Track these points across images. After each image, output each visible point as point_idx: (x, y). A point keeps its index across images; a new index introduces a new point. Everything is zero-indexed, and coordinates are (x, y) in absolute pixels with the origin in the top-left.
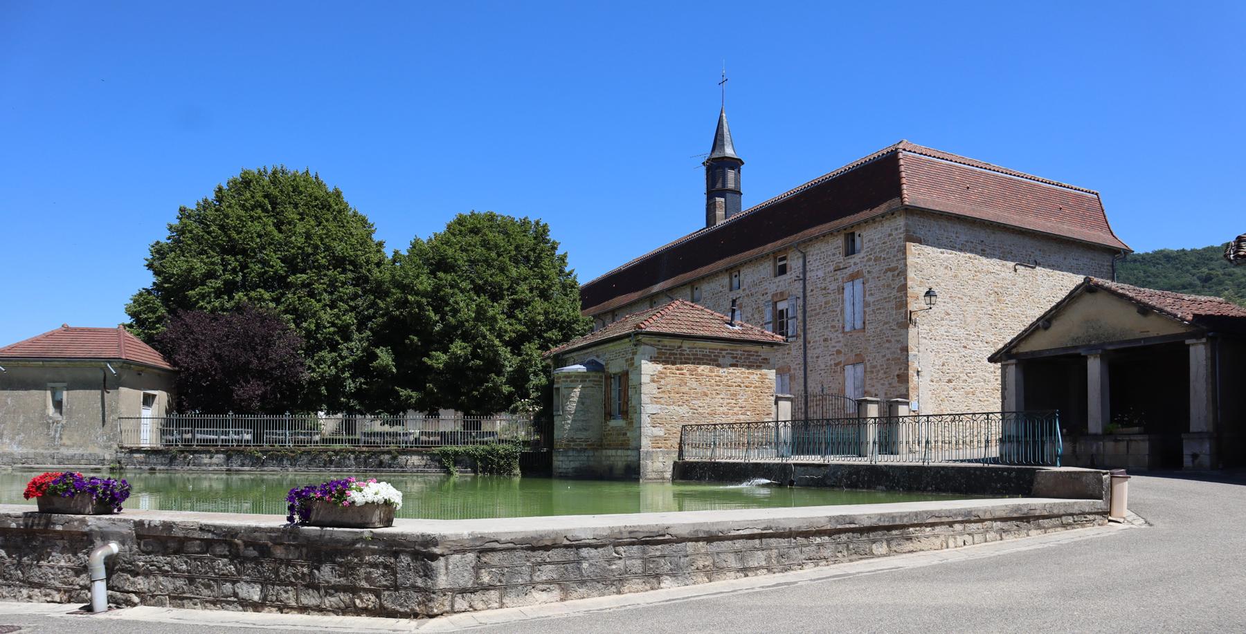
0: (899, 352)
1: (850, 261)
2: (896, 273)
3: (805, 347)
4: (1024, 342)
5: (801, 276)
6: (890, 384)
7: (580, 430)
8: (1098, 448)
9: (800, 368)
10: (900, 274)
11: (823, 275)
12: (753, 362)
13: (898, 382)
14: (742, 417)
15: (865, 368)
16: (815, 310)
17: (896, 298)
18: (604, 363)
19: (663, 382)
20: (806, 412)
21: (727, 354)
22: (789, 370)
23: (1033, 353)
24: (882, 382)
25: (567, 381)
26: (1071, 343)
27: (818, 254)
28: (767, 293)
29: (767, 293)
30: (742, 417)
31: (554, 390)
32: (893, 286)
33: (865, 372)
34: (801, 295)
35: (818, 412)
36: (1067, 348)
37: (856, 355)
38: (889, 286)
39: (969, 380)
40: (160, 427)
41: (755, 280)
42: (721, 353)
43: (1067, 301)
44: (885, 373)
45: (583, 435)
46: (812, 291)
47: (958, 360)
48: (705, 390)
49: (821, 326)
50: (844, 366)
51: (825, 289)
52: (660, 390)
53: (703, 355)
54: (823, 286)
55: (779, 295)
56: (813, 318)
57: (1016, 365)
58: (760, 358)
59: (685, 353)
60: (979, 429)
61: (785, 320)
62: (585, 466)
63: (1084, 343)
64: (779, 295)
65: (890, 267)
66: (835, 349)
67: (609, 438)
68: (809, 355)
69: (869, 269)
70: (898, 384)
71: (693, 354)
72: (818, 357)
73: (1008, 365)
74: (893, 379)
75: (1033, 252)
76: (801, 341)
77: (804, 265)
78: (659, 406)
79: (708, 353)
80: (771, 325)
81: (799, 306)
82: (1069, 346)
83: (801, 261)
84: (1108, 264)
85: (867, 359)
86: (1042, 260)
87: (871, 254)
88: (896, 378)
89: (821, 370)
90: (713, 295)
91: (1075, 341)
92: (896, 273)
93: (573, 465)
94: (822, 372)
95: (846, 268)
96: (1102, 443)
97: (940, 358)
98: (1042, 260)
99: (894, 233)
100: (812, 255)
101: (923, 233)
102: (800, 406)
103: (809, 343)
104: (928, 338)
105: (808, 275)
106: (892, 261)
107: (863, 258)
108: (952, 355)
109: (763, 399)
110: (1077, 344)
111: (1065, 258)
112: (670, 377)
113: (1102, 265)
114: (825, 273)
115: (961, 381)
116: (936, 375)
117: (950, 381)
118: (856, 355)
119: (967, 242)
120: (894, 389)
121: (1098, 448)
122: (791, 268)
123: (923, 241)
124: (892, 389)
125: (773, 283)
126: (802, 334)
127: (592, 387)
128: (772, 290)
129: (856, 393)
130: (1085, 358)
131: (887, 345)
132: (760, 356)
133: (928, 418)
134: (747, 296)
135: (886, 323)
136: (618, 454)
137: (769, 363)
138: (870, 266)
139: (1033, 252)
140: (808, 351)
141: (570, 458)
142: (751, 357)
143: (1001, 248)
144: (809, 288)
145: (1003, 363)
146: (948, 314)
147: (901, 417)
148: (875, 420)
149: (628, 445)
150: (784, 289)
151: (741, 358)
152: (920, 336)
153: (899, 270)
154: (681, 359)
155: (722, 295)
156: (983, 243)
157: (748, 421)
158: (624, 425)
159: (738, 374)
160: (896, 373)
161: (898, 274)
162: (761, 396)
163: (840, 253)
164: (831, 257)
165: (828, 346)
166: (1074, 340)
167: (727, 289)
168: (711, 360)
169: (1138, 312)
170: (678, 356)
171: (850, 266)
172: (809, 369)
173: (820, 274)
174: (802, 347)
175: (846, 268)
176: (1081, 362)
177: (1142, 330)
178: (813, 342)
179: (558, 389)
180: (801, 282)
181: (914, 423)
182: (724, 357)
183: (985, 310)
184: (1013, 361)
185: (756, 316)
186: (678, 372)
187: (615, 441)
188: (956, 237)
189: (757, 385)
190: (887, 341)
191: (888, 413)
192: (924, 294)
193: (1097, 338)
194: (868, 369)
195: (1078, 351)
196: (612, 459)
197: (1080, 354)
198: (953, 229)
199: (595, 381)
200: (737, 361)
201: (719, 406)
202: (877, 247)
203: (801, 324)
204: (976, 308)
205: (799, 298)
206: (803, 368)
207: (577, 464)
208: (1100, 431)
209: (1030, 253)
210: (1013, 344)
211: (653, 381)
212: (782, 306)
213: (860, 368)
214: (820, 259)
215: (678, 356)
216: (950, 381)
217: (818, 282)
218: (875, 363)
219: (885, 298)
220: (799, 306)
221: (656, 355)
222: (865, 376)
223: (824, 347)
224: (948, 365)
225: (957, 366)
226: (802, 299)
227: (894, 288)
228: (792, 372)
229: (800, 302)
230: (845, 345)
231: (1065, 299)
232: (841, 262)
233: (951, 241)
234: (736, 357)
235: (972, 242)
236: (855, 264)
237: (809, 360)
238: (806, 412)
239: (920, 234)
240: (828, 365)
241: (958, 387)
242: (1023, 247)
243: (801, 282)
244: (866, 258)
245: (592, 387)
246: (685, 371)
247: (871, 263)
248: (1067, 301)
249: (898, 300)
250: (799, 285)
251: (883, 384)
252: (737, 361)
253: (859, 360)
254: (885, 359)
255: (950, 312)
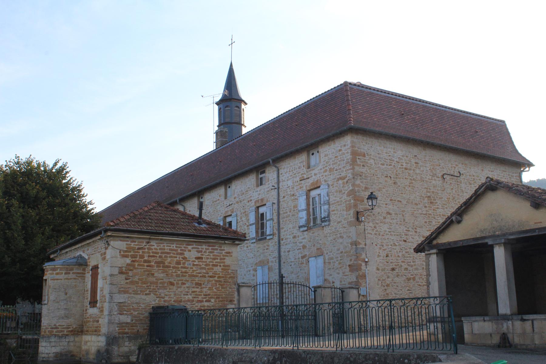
0: (350, 246)
1: (311, 172)
2: (345, 181)
3: (279, 243)
4: (442, 234)
5: (276, 186)
6: (343, 273)
7: (63, 318)
8: (508, 328)
9: (275, 261)
10: (349, 181)
11: (292, 184)
12: (217, 256)
13: (350, 271)
14: (206, 304)
15: (324, 260)
16: (287, 212)
17: (346, 202)
18: (87, 257)
19: (131, 273)
20: (281, 297)
21: (192, 248)
22: (268, 262)
23: (449, 243)
24: (338, 271)
25: (53, 274)
26: (479, 234)
27: (287, 167)
28: (251, 200)
29: (251, 200)
30: (206, 304)
31: (44, 281)
32: (343, 192)
33: (324, 263)
34: (276, 201)
35: (290, 296)
36: (474, 239)
37: (317, 249)
38: (341, 191)
39: (410, 268)
40: (327, 296)
41: (243, 190)
42: (187, 248)
43: (474, 198)
44: (340, 263)
45: (64, 323)
46: (284, 197)
47: (400, 252)
48: (172, 280)
49: (291, 226)
50: (308, 259)
51: (293, 195)
52: (128, 281)
53: (170, 249)
54: (292, 193)
55: (260, 201)
56: (285, 220)
57: (437, 253)
58: (224, 252)
59: (153, 247)
60: (427, 311)
61: (265, 221)
62: (65, 350)
63: (490, 234)
64: (260, 201)
65: (340, 176)
66: (302, 245)
67: (87, 324)
68: (282, 250)
69: (325, 178)
70: (350, 273)
71: (160, 249)
72: (289, 251)
73: (430, 254)
74: (345, 268)
75: (457, 165)
76: (276, 238)
77: (278, 177)
78: (126, 296)
79: (175, 248)
80: (254, 226)
81: (275, 210)
82: (478, 236)
83: (276, 173)
84: (516, 175)
85: (325, 252)
86: (464, 171)
87: (326, 167)
88: (348, 267)
89: (292, 262)
90: (213, 202)
91: (483, 232)
92: (345, 181)
93: (54, 350)
94: (293, 264)
95: (309, 178)
96: (511, 322)
97: (384, 250)
98: (464, 171)
99: (343, 149)
100: (284, 169)
101: (366, 148)
102: (290, 293)
103: (282, 240)
104: (373, 233)
105: (281, 184)
106: (342, 171)
107: (321, 169)
108: (394, 247)
109: (226, 287)
110: (484, 235)
111: (483, 170)
112: (138, 268)
113: (512, 176)
114: (293, 183)
115: (403, 270)
116: (381, 265)
117: (393, 269)
118: (317, 249)
119: (403, 156)
120: (347, 277)
121: (508, 328)
122: (268, 179)
123: (366, 154)
124: (345, 277)
125: (256, 192)
126: (277, 232)
127: (75, 279)
128: (255, 198)
129: (318, 280)
130: (492, 247)
131: (341, 240)
132: (224, 250)
133: (391, 302)
134: (237, 202)
135: (339, 222)
136: (93, 340)
137: (231, 256)
138: (326, 176)
139: (457, 165)
140: (281, 247)
141: (53, 344)
142: (215, 251)
143: (431, 161)
144: (282, 195)
145: (426, 252)
146: (390, 214)
147: (242, 308)
148: (340, 305)
149: (100, 331)
150: (264, 196)
151: (205, 252)
152: (366, 232)
153: (347, 178)
154: (149, 253)
155: (219, 203)
156: (416, 158)
157: (219, 308)
158: (98, 313)
159: (203, 266)
160: (348, 263)
161: (347, 182)
162: (224, 284)
163: (304, 166)
164: (298, 170)
165: (296, 242)
166: (482, 231)
167: (223, 198)
168: (177, 254)
169: (531, 206)
170: (146, 250)
171: (312, 176)
172: (282, 262)
173: (290, 183)
174: (277, 243)
175: (309, 178)
176: (490, 249)
177: (536, 222)
178: (286, 239)
179: (46, 280)
180: (276, 190)
181: (377, 308)
182: (190, 251)
183: (420, 211)
184: (434, 251)
185: (243, 219)
186: (146, 264)
187: (91, 327)
188: (394, 152)
189: (221, 275)
190: (340, 237)
191: (313, 301)
192: (367, 197)
193: (501, 229)
194: (327, 261)
195: (486, 241)
196: (88, 344)
197: (487, 243)
198: (391, 146)
199: (78, 273)
200: (203, 255)
201: (184, 295)
202: (331, 161)
203: (276, 225)
204: (413, 209)
205: (274, 203)
206: (277, 261)
207: (57, 350)
208: (508, 312)
209: (454, 166)
210: (432, 237)
211: (121, 273)
212: (261, 210)
213: (320, 260)
214: (290, 171)
215: (146, 250)
216: (393, 269)
217: (288, 190)
218: (332, 256)
219: (338, 202)
220: (275, 210)
221: (125, 249)
222: (324, 267)
223: (293, 243)
224: (391, 256)
225: (398, 256)
226: (276, 204)
227: (344, 193)
228: (270, 264)
229: (275, 206)
230: (309, 241)
231: (471, 197)
232: (305, 174)
233: (390, 156)
234: (201, 251)
235: (407, 157)
236: (315, 175)
237: (282, 254)
238: (281, 297)
239: (364, 149)
240: (297, 257)
241: (400, 274)
242: (449, 161)
243: (276, 190)
244: (323, 170)
245: (75, 279)
246: (153, 264)
247: (326, 174)
248: (474, 198)
249: (348, 203)
250: (275, 193)
251: (338, 274)
252: (203, 255)
253: (320, 253)
254: (339, 252)
255: (391, 212)
